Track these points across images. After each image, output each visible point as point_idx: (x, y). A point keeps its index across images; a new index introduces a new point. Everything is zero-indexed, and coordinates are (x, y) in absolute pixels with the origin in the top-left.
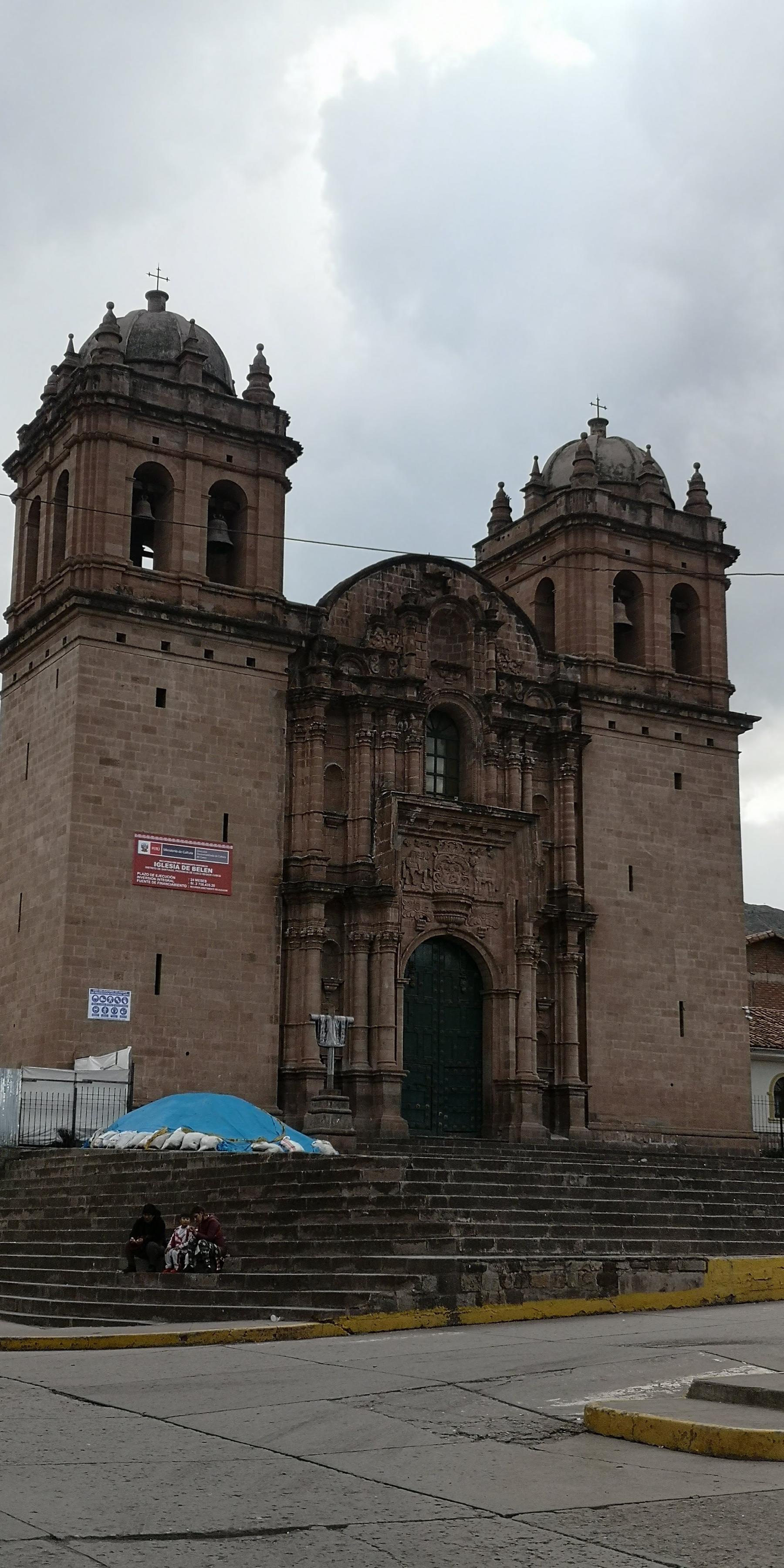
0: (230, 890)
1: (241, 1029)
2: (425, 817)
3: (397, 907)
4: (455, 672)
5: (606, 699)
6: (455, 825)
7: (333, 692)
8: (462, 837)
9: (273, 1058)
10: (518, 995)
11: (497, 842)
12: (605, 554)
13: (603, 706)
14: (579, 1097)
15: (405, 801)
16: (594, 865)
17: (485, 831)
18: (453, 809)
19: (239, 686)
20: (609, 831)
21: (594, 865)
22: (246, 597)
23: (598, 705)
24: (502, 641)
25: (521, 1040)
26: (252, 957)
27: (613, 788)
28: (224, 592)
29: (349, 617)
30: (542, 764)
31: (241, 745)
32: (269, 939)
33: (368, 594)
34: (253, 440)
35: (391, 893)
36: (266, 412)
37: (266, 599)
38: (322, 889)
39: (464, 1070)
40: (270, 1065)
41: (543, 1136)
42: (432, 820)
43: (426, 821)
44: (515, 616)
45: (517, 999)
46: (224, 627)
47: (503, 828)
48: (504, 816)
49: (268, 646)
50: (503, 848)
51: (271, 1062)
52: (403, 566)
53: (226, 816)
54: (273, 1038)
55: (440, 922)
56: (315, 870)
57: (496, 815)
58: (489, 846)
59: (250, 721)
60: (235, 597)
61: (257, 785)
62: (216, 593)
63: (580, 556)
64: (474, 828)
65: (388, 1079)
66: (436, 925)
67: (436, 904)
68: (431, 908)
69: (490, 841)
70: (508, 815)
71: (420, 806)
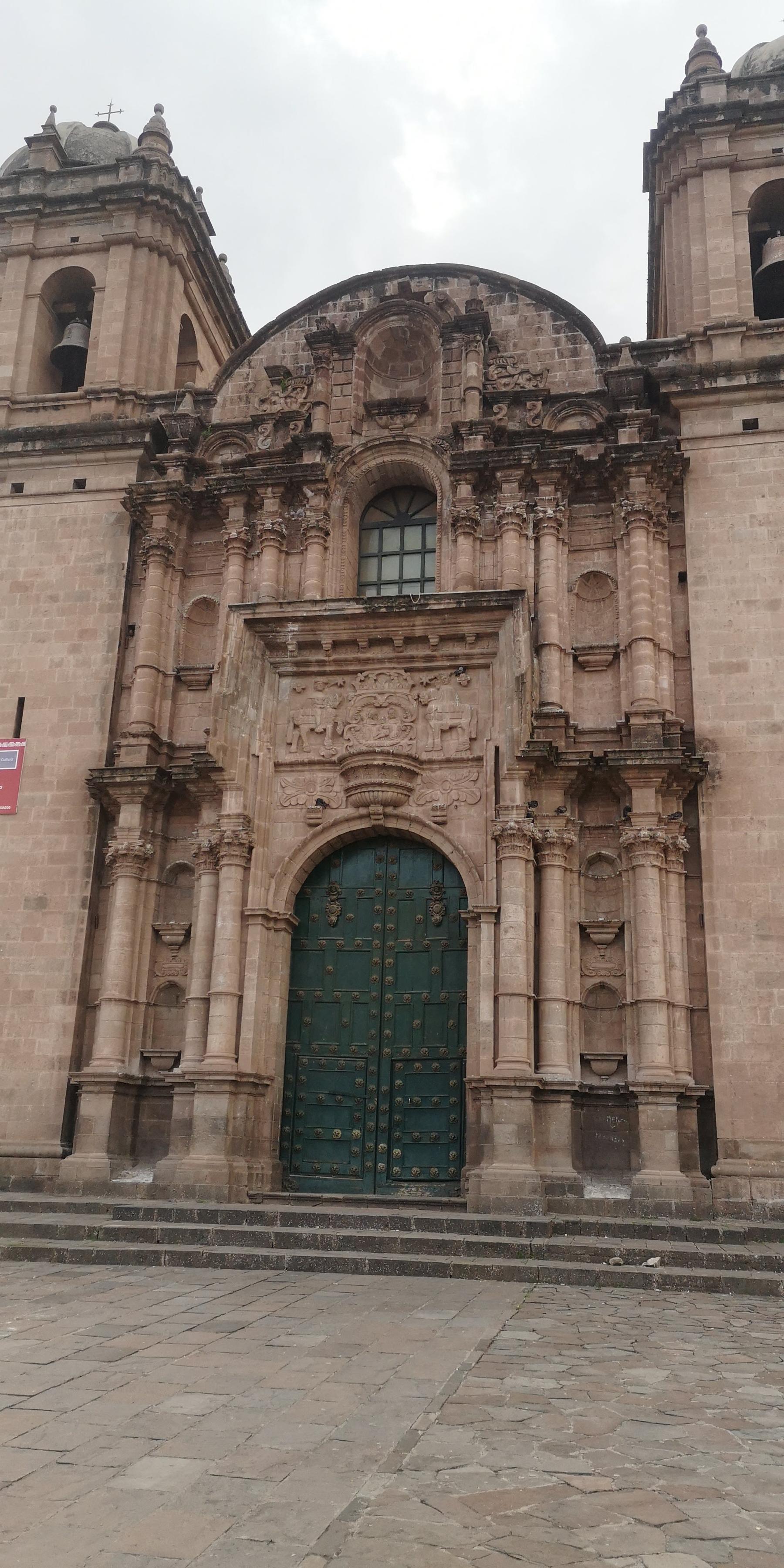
0: (14, 805)
1: (13, 1016)
2: (309, 638)
3: (238, 789)
4: (403, 413)
5: (722, 382)
6: (373, 643)
7: (165, 486)
8: (399, 660)
9: (61, 1060)
10: (497, 915)
11: (469, 656)
12: (720, 166)
13: (723, 397)
14: (660, 1108)
15: (257, 616)
16: (715, 669)
17: (434, 641)
18: (349, 612)
19: (58, 519)
20: (748, 603)
21: (715, 669)
22: (79, 402)
23: (712, 398)
24: (524, 355)
25: (501, 999)
26: (41, 903)
27: (757, 529)
28: (47, 404)
29: (251, 391)
30: (600, 521)
31: (54, 599)
32: (73, 872)
33: (284, 352)
34: (98, 205)
35: (210, 765)
36: (127, 168)
37: (103, 395)
38: (118, 780)
39: (435, 1064)
40: (55, 1073)
41: (535, 1191)
42: (326, 641)
43: (316, 645)
44: (550, 311)
45: (497, 924)
46: (25, 445)
47: (467, 629)
48: (454, 606)
49: (100, 455)
50: (487, 667)
51: (56, 1067)
52: (346, 298)
53: (21, 701)
54: (65, 1027)
55: (357, 806)
56: (127, 754)
57: (436, 607)
58: (457, 667)
59: (72, 563)
60: (64, 406)
61: (75, 649)
62: (37, 409)
63: (681, 188)
64: (409, 640)
65: (204, 1087)
66: (351, 811)
67: (344, 774)
68: (339, 785)
69: (455, 657)
70: (459, 603)
71: (295, 620)
